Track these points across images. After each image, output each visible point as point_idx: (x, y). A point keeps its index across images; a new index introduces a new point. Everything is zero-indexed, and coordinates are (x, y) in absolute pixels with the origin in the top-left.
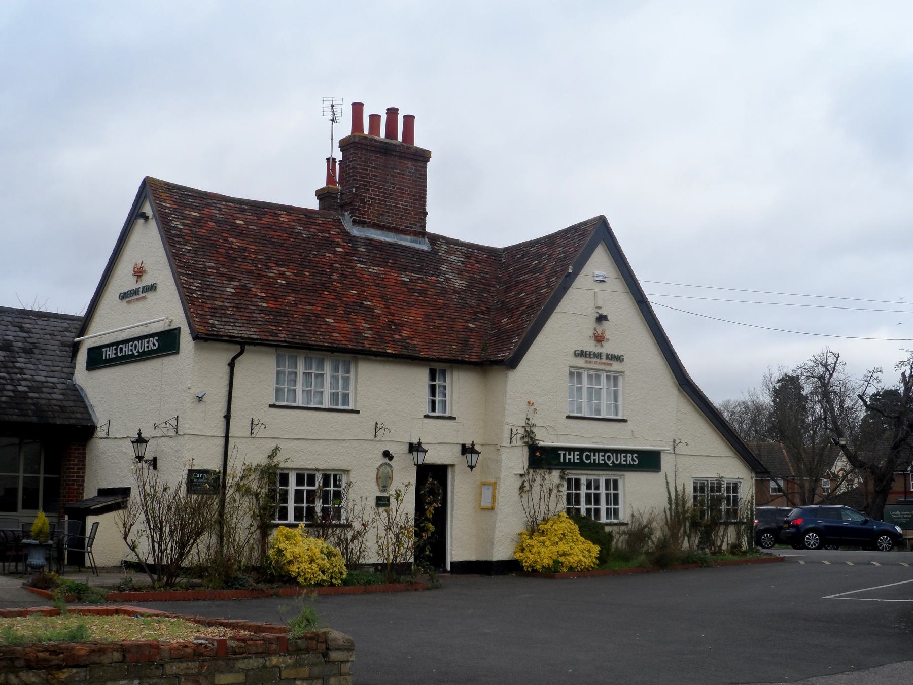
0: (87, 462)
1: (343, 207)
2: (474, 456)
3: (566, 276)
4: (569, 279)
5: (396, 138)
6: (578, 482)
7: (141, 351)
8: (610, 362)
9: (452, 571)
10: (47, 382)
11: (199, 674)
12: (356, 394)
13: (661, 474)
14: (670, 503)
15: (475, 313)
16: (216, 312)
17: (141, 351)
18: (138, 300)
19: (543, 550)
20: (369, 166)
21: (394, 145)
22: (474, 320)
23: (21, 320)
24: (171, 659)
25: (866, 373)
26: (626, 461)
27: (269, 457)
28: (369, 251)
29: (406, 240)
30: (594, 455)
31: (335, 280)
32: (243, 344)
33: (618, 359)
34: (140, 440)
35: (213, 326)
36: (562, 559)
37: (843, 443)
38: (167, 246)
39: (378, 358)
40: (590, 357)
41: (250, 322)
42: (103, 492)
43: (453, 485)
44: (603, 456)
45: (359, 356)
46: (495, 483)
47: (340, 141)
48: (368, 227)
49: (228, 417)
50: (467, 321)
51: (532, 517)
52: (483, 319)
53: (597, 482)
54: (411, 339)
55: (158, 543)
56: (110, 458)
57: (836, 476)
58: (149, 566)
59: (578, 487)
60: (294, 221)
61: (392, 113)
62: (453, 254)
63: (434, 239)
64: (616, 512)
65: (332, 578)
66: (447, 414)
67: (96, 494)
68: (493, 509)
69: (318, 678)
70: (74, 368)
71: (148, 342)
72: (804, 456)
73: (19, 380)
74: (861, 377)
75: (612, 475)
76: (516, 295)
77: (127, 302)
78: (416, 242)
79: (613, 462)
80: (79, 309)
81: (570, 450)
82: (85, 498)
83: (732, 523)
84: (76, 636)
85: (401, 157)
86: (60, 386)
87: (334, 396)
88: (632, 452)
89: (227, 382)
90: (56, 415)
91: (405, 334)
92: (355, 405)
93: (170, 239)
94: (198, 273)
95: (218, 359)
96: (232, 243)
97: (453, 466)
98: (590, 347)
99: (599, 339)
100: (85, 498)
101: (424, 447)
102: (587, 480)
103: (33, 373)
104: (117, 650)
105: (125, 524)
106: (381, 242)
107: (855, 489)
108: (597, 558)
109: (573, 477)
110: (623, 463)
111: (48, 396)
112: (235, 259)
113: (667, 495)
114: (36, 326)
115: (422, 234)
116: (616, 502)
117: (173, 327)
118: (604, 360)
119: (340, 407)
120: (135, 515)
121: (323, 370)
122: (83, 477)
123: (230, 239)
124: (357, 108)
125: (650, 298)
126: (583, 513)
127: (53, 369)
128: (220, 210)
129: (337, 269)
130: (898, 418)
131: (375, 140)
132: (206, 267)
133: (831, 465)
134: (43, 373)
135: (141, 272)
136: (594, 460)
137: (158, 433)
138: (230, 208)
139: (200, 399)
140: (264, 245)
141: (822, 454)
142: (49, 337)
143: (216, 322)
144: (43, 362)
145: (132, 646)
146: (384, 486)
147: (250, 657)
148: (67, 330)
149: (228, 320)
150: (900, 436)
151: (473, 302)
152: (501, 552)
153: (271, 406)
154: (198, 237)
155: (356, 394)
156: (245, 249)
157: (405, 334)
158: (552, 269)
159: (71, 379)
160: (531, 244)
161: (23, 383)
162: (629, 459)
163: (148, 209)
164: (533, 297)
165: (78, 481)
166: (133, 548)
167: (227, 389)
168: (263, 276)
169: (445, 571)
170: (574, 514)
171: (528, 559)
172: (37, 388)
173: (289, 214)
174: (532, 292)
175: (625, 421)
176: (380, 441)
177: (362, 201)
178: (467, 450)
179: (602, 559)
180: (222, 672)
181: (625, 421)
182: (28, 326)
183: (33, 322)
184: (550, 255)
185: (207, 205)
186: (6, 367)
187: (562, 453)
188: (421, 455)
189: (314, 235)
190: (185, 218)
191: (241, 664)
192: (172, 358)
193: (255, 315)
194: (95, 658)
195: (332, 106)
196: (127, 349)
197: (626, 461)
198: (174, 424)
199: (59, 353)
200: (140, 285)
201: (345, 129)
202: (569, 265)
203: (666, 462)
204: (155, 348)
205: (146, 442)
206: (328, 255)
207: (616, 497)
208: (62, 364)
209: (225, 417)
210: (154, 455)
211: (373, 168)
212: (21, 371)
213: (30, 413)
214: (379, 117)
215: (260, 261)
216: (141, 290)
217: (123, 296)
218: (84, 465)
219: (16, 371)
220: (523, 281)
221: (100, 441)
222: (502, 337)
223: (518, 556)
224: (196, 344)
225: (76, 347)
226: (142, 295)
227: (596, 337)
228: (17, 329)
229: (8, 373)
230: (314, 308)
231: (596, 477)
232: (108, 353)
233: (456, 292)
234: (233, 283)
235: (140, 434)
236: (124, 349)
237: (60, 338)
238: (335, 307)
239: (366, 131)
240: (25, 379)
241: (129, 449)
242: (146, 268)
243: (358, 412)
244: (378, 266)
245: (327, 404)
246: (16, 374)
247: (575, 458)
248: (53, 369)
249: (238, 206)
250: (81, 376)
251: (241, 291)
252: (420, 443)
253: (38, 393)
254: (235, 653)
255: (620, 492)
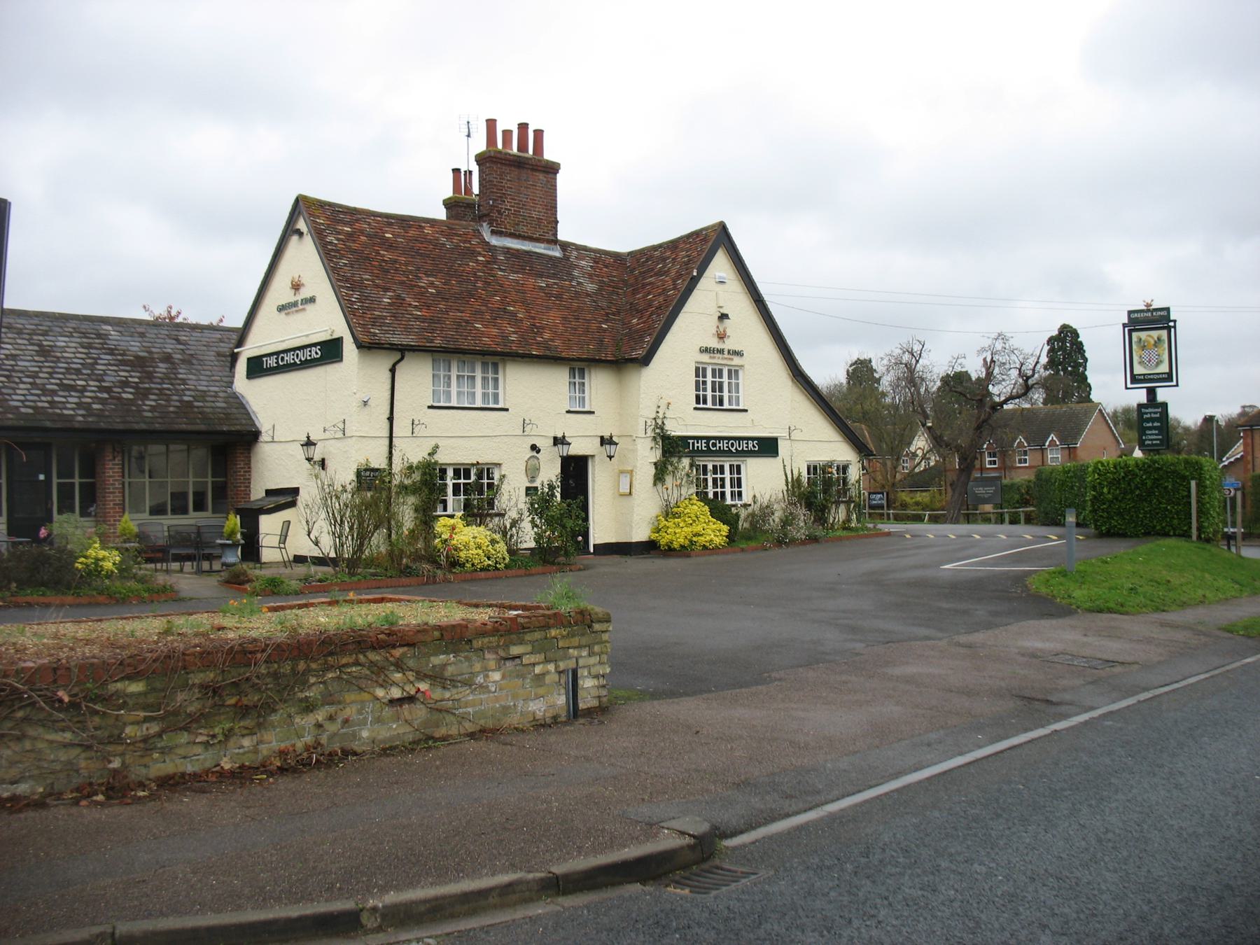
0: (252, 465)
1: (481, 218)
2: (613, 447)
3: (691, 279)
4: (694, 282)
5: (527, 151)
6: (705, 467)
7: (303, 359)
8: (731, 357)
9: (594, 553)
10: (209, 391)
11: (498, 646)
12: (505, 393)
13: (779, 459)
14: (787, 485)
15: (607, 314)
16: (375, 321)
17: (303, 359)
18: (297, 311)
19: (678, 530)
20: (503, 179)
21: (524, 157)
22: (606, 321)
23: (176, 333)
24: (477, 634)
25: (951, 359)
26: (747, 447)
27: (429, 454)
28: (507, 259)
29: (540, 248)
30: (698, 443)
31: (479, 288)
32: (403, 351)
33: (738, 354)
34: (309, 443)
35: (375, 335)
36: (695, 539)
37: (930, 424)
38: (325, 261)
39: (525, 359)
40: (714, 353)
41: (407, 330)
42: (269, 493)
43: (593, 474)
44: (727, 443)
45: (507, 358)
46: (632, 471)
47: (476, 156)
48: (505, 236)
49: (391, 419)
50: (601, 323)
51: (666, 501)
52: (614, 320)
53: (722, 467)
54: (552, 340)
55: (339, 538)
56: (277, 461)
57: (914, 455)
58: (332, 559)
59: (705, 473)
60: (437, 233)
61: (523, 127)
62: (583, 260)
63: (565, 246)
64: (740, 494)
65: (496, 563)
66: (586, 409)
67: (264, 495)
68: (630, 493)
69: (585, 646)
70: (234, 377)
71: (310, 351)
72: (885, 436)
73: (183, 390)
74: (946, 363)
75: (735, 462)
76: (644, 297)
77: (286, 314)
78: (549, 249)
79: (736, 449)
80: (236, 320)
81: (698, 438)
82: (252, 499)
83: (843, 502)
84: (390, 620)
85: (533, 170)
86: (221, 394)
87: (485, 395)
88: (753, 439)
89: (389, 386)
90: (222, 422)
91: (547, 336)
92: (505, 404)
93: (328, 254)
94: (355, 285)
95: (379, 367)
96: (383, 256)
97: (593, 456)
98: (714, 343)
99: (722, 337)
100: (252, 499)
101: (568, 440)
102: (713, 466)
103: (196, 383)
104: (436, 630)
105: (307, 522)
106: (518, 250)
107: (933, 466)
108: (727, 537)
109: (701, 463)
110: (745, 449)
111: (213, 404)
112: (388, 271)
113: (784, 478)
114: (192, 338)
115: (555, 241)
116: (739, 486)
117: (335, 336)
118: (726, 356)
119: (491, 406)
120: (317, 513)
121: (474, 372)
122: (249, 479)
123: (382, 252)
124: (491, 124)
125: (766, 298)
126: (711, 496)
127: (213, 378)
128: (369, 224)
129: (480, 277)
130: (981, 400)
131: (509, 154)
132: (362, 279)
133: (910, 444)
134: (205, 383)
135: (298, 285)
136: (720, 447)
137: (328, 435)
138: (378, 222)
139: (365, 403)
140: (413, 257)
141: (903, 434)
142: (205, 348)
143: (377, 331)
144: (202, 372)
145: (447, 626)
146: (533, 477)
147: (535, 631)
148: (221, 341)
149: (387, 328)
150: (983, 417)
151: (605, 304)
152: (640, 534)
153: (429, 407)
154: (353, 251)
155: (505, 393)
156: (395, 261)
157: (547, 336)
158: (677, 272)
159: (231, 387)
160: (655, 248)
161: (188, 393)
162: (750, 446)
163: (301, 225)
164: (661, 299)
165: (244, 483)
166: (316, 543)
167: (389, 392)
168: (415, 286)
169: (589, 553)
170: (702, 496)
171: (664, 540)
172: (203, 396)
173: (432, 226)
174: (660, 295)
175: (746, 411)
176: (528, 435)
177: (499, 212)
178: (604, 441)
179: (731, 537)
180: (514, 644)
181: (746, 411)
182: (185, 338)
183: (188, 334)
184: (673, 259)
185: (357, 220)
186: (169, 379)
187: (691, 441)
188: (565, 447)
189: (458, 246)
190: (339, 233)
191: (528, 637)
192: (336, 366)
193: (411, 323)
194: (420, 637)
195: (468, 123)
196: (289, 358)
197: (747, 447)
198: (342, 427)
199: (216, 363)
200: (299, 298)
201: (480, 145)
202: (693, 268)
203: (782, 446)
204: (318, 356)
205: (315, 444)
206: (471, 264)
207: (739, 480)
208: (220, 374)
209: (388, 419)
210: (322, 457)
211: (508, 180)
212: (184, 382)
213: (198, 421)
214: (511, 131)
215: (411, 272)
216: (300, 303)
217: (281, 309)
218: (249, 468)
219: (178, 382)
220: (651, 283)
221: (265, 445)
222: (635, 336)
223: (654, 536)
224: (359, 352)
225: (234, 358)
226: (300, 307)
227: (718, 335)
228: (174, 342)
229: (172, 384)
230: (464, 314)
231: (721, 463)
232: (269, 362)
233: (588, 295)
234: (388, 294)
235: (308, 437)
236: (286, 358)
237: (215, 349)
238: (482, 313)
239: (500, 146)
240: (188, 390)
241: (300, 453)
242: (303, 281)
243: (507, 410)
244: (517, 273)
245: (479, 404)
246: (180, 385)
247: (702, 445)
248: (213, 378)
249: (385, 220)
250: (241, 383)
251: (398, 302)
252: (564, 437)
253: (202, 402)
254: (524, 628)
255: (743, 476)
